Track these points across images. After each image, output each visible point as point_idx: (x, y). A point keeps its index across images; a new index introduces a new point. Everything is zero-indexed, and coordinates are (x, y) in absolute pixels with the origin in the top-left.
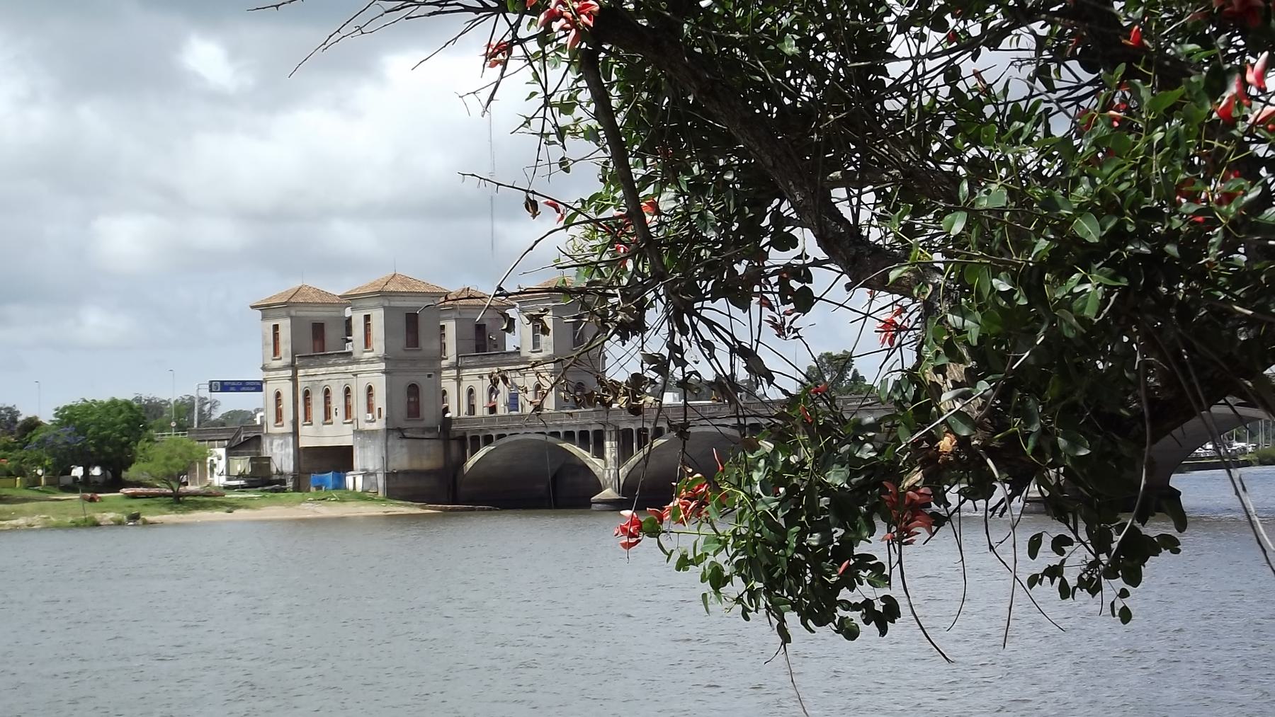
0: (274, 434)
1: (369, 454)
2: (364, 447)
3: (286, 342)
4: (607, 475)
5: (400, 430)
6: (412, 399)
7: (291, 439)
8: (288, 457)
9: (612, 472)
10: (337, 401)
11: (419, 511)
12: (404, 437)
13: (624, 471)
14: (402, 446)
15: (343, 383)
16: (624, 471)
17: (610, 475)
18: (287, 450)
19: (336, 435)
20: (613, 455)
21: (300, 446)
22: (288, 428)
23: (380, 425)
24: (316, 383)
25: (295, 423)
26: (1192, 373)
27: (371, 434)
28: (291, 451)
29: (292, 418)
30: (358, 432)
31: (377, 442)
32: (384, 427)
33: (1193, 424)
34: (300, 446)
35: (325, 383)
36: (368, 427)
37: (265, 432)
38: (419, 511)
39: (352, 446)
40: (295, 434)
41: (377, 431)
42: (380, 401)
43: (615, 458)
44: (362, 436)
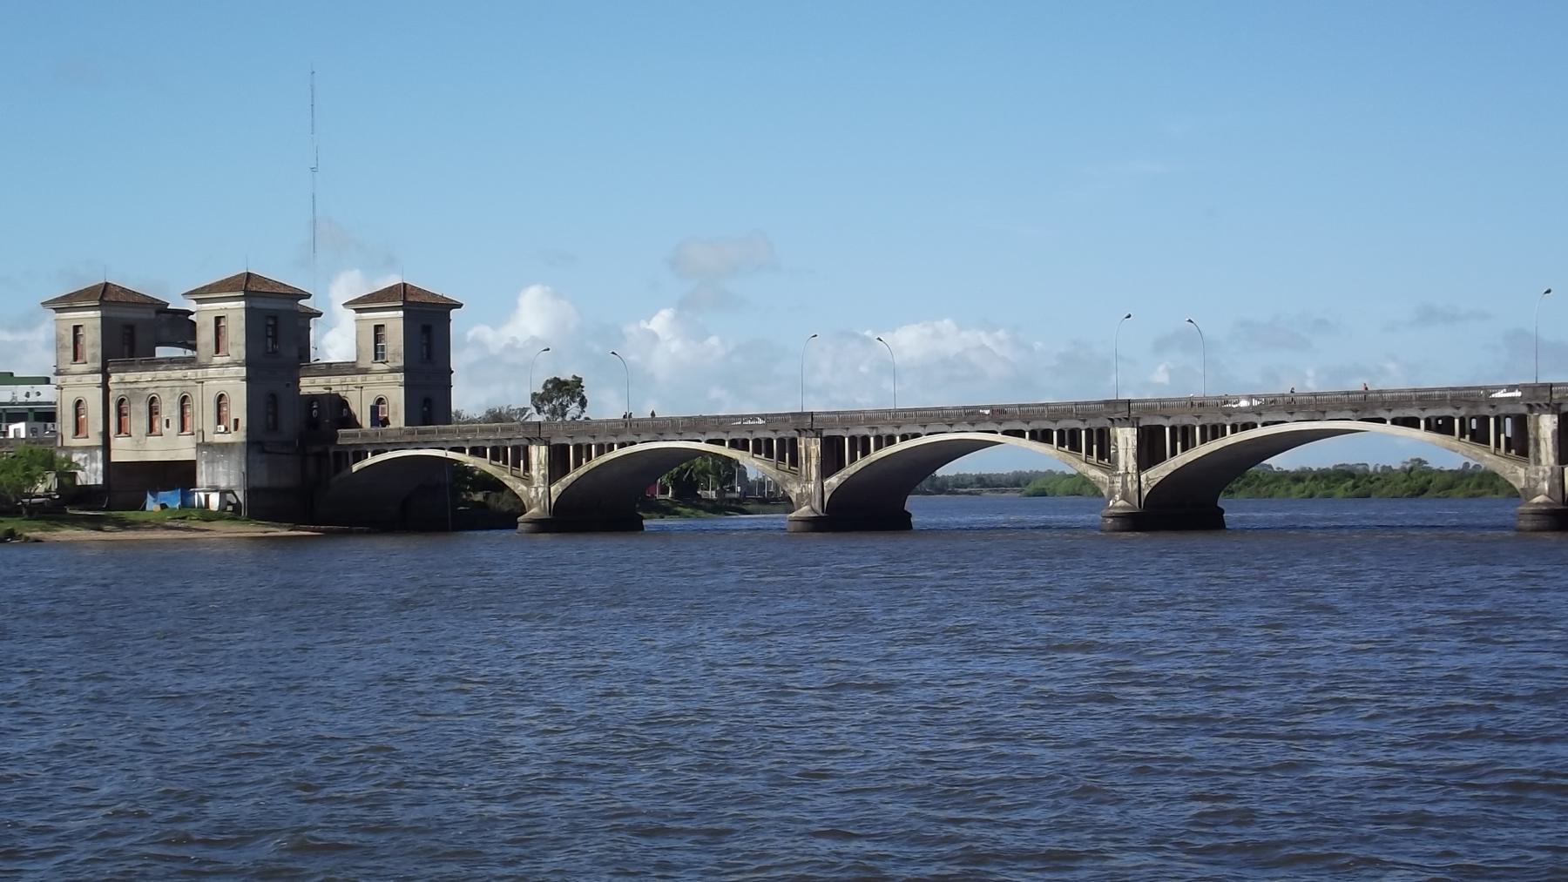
0: (74, 448)
1: (221, 469)
2: (213, 462)
3: (93, 345)
4: (533, 494)
5: (259, 443)
6: (425, 409)
7: (99, 454)
8: (95, 473)
9: (541, 490)
10: (169, 409)
11: (285, 533)
12: (264, 451)
13: (557, 489)
15: (178, 391)
16: (557, 489)
17: (537, 493)
18: (94, 465)
19: (171, 447)
20: (542, 472)
21: (113, 460)
22: (95, 439)
23: (238, 437)
24: (137, 391)
25: (106, 434)
26: (982, 868)
27: (225, 448)
28: (100, 466)
29: (101, 429)
30: (202, 446)
31: (233, 456)
32: (244, 440)
33: (1552, 507)
34: (113, 460)
35: (151, 391)
36: (219, 439)
37: (59, 444)
38: (285, 533)
39: (195, 461)
40: (106, 447)
41: (233, 444)
42: (238, 408)
43: (544, 475)
44: (210, 449)
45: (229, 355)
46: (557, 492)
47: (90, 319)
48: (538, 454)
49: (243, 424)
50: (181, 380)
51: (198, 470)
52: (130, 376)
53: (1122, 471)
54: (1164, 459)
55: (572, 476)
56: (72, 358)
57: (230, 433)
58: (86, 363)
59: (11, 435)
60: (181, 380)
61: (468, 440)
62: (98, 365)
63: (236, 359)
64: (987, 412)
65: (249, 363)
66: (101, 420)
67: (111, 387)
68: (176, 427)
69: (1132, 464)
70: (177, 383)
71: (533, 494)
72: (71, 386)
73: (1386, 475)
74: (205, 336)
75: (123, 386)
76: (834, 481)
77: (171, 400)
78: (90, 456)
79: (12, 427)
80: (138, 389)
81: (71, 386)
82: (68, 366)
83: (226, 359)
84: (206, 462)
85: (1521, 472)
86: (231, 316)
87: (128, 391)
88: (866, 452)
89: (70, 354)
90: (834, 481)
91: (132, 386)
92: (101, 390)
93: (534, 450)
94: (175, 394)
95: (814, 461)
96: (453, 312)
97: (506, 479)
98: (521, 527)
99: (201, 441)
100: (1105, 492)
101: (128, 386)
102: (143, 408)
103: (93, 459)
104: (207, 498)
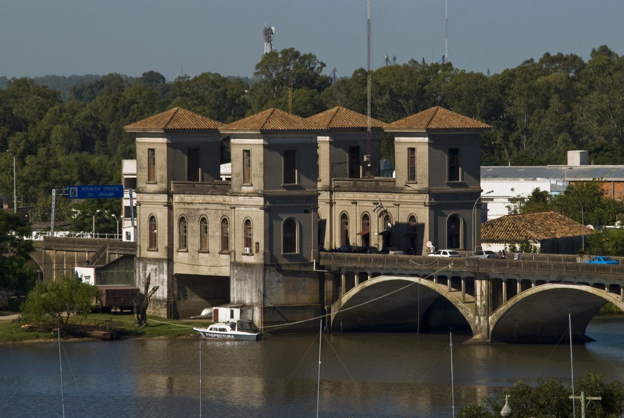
2: (241, 280)
3: (161, 168)
7: (165, 265)
13: (494, 318)
14: (278, 281)
15: (220, 214)
18: (161, 276)
20: (484, 302)
22: (161, 254)
25: (170, 250)
27: (247, 266)
32: (262, 262)
40: (170, 260)
45: (252, 186)
46: (493, 322)
48: (480, 286)
50: (221, 204)
51: (232, 287)
52: (188, 198)
55: (502, 309)
56: (147, 177)
57: (253, 255)
58: (156, 184)
60: (221, 204)
61: (396, 269)
62: (164, 186)
63: (257, 189)
66: (166, 236)
67: (175, 206)
68: (219, 242)
70: (220, 207)
72: (147, 203)
75: (183, 206)
77: (215, 222)
78: (159, 267)
80: (194, 209)
82: (144, 185)
83: (250, 189)
84: (237, 280)
86: (158, 149)
87: (186, 211)
88: (511, 293)
91: (190, 207)
92: (166, 209)
93: (478, 283)
94: (218, 216)
97: (460, 306)
99: (233, 260)
101: (187, 206)
103: (161, 271)
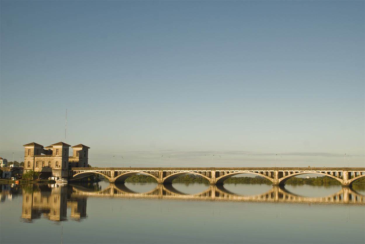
15: (48, 161)
16: (116, 178)
23: (60, 168)
25: (34, 167)
29: (33, 166)
36: (56, 168)
42: (60, 164)
47: (32, 148)
49: (61, 166)
53: (213, 178)
54: (219, 176)
59: (11, 167)
62: (33, 156)
64: (42, 154)
65: (63, 157)
69: (214, 177)
70: (48, 159)
71: (111, 179)
73: (268, 181)
74: (54, 152)
76: (165, 178)
79: (11, 165)
81: (28, 159)
85: (273, 179)
88: (171, 174)
89: (27, 154)
90: (165, 178)
92: (33, 160)
95: (161, 175)
96: (89, 149)
98: (57, 181)
100: (210, 181)
102: (41, 163)
104: (55, 178)
